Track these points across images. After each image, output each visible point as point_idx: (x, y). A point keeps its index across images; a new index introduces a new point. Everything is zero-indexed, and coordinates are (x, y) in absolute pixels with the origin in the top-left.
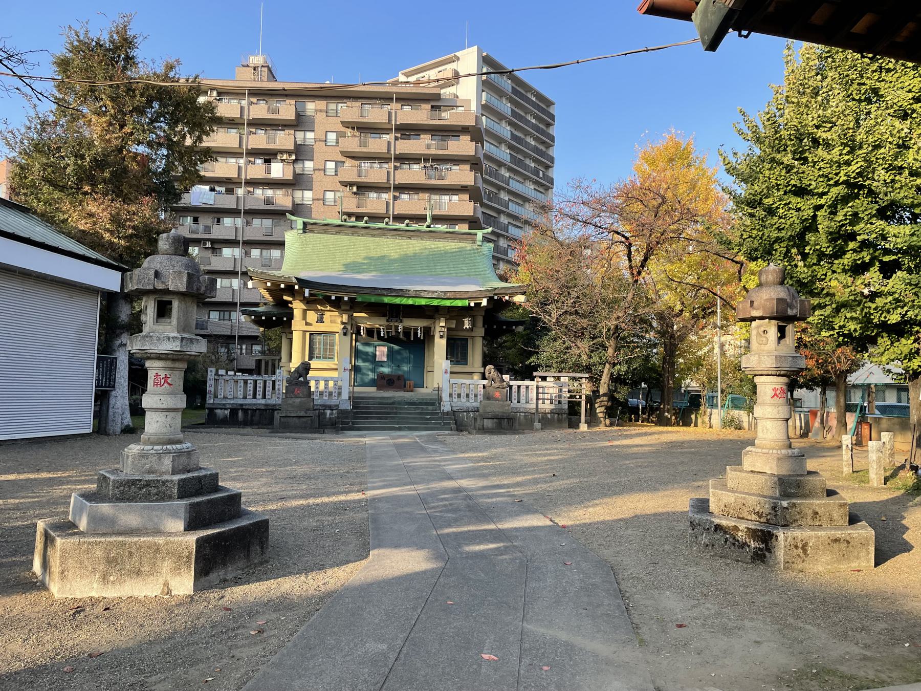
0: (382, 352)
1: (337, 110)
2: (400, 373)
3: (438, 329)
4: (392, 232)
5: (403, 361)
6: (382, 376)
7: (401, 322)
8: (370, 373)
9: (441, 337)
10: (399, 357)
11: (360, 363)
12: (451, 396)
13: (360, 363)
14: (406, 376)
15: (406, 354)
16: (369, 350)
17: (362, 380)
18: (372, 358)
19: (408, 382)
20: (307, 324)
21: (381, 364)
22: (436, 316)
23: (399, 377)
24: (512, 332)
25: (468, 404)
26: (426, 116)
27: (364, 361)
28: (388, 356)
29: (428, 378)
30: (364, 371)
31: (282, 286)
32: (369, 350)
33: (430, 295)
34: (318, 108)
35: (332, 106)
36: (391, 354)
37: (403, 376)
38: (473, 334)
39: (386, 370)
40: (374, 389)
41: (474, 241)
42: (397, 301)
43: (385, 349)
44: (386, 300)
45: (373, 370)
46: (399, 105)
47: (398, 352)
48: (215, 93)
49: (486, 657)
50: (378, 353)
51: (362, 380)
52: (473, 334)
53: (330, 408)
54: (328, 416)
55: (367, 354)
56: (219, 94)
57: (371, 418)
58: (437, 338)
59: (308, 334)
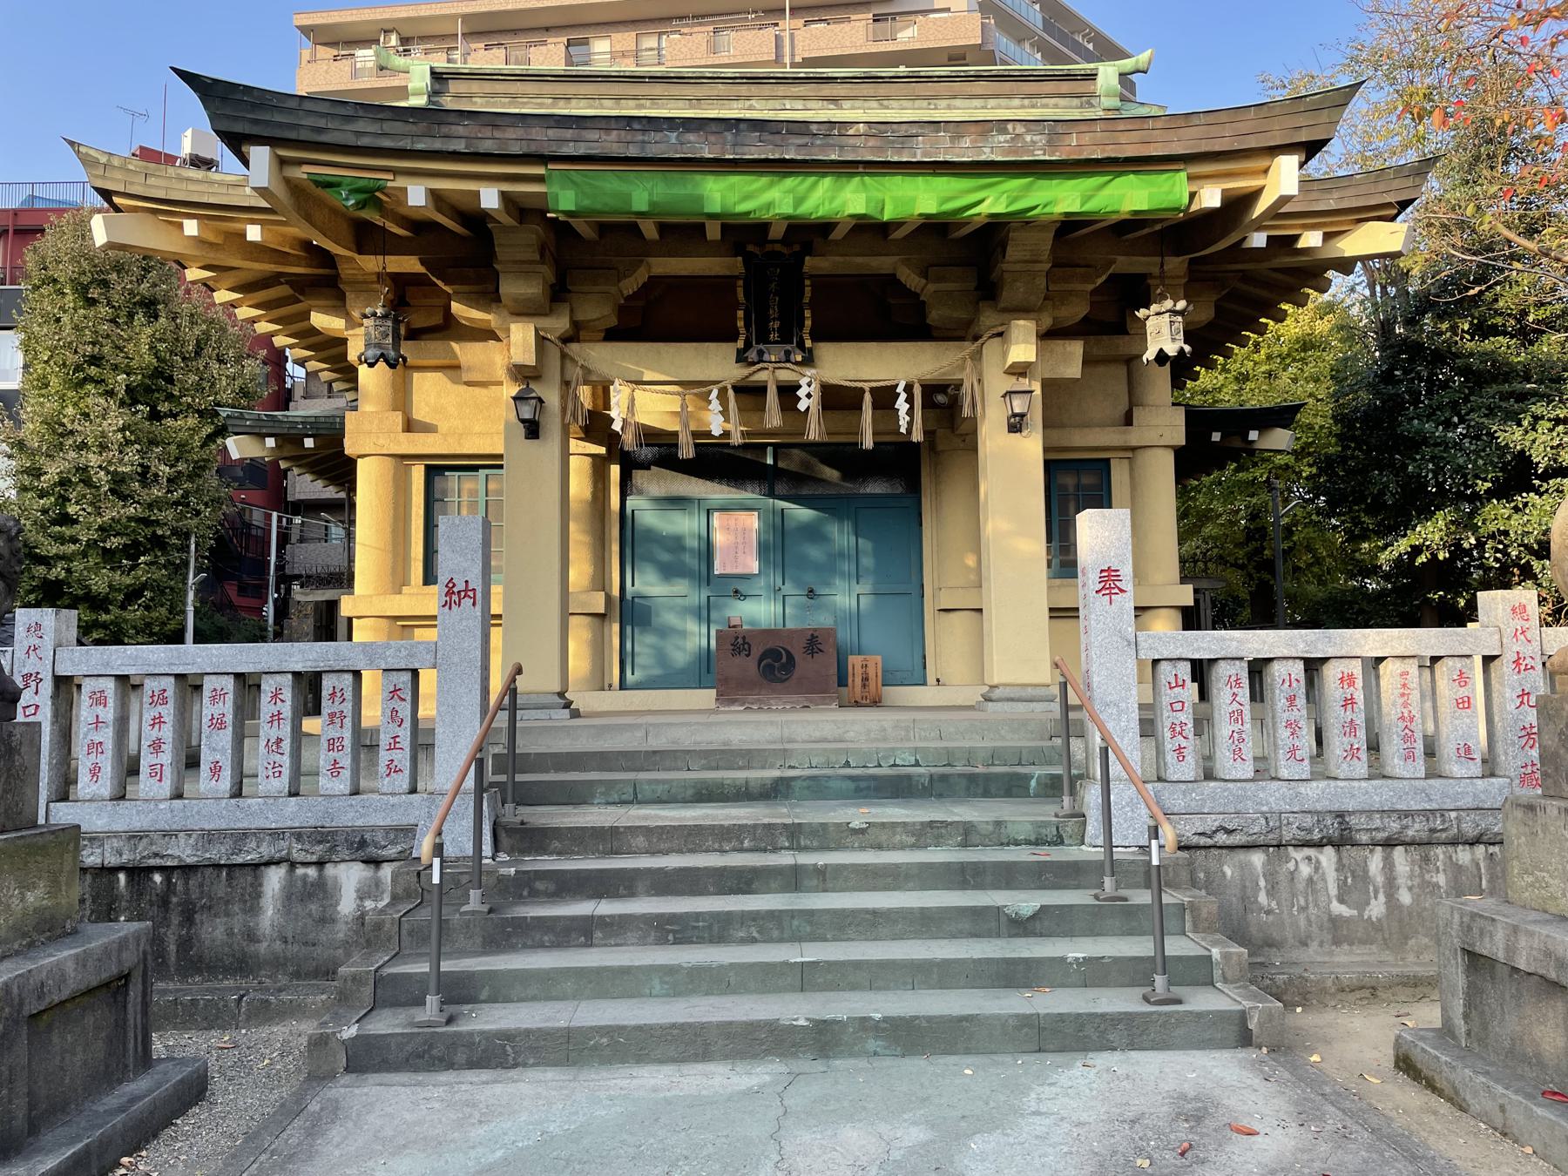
0: (735, 528)
1: (659, 49)
2: (823, 620)
3: (997, 383)
4: (766, 90)
5: (828, 569)
6: (737, 642)
7: (809, 361)
8: (692, 626)
9: (1016, 425)
10: (815, 552)
11: (647, 583)
12: (1148, 728)
13: (647, 583)
14: (845, 635)
15: (841, 535)
16: (684, 524)
17: (661, 658)
18: (696, 562)
19: (855, 661)
20: (410, 426)
21: (736, 587)
22: (988, 319)
23: (814, 642)
24: (1250, 454)
25: (1272, 796)
26: (862, 32)
27: (669, 572)
28: (764, 550)
29: (946, 643)
30: (671, 619)
31: (1299, 1010)
32: (684, 524)
33: (965, 150)
34: (618, 48)
35: (651, 42)
36: (778, 546)
37: (830, 633)
38: (1134, 437)
39: (759, 611)
40: (705, 697)
41: (1088, 98)
42: (774, 199)
43: (752, 521)
44: (723, 195)
45: (704, 614)
46: (800, 22)
47: (812, 533)
48: (394, 40)
49: (770, 461)
50: (719, 538)
51: (661, 658)
52: (1134, 437)
53: (363, 849)
54: (347, 905)
55: (676, 543)
56: (405, 41)
57: (615, 929)
58: (992, 437)
59: (418, 473)
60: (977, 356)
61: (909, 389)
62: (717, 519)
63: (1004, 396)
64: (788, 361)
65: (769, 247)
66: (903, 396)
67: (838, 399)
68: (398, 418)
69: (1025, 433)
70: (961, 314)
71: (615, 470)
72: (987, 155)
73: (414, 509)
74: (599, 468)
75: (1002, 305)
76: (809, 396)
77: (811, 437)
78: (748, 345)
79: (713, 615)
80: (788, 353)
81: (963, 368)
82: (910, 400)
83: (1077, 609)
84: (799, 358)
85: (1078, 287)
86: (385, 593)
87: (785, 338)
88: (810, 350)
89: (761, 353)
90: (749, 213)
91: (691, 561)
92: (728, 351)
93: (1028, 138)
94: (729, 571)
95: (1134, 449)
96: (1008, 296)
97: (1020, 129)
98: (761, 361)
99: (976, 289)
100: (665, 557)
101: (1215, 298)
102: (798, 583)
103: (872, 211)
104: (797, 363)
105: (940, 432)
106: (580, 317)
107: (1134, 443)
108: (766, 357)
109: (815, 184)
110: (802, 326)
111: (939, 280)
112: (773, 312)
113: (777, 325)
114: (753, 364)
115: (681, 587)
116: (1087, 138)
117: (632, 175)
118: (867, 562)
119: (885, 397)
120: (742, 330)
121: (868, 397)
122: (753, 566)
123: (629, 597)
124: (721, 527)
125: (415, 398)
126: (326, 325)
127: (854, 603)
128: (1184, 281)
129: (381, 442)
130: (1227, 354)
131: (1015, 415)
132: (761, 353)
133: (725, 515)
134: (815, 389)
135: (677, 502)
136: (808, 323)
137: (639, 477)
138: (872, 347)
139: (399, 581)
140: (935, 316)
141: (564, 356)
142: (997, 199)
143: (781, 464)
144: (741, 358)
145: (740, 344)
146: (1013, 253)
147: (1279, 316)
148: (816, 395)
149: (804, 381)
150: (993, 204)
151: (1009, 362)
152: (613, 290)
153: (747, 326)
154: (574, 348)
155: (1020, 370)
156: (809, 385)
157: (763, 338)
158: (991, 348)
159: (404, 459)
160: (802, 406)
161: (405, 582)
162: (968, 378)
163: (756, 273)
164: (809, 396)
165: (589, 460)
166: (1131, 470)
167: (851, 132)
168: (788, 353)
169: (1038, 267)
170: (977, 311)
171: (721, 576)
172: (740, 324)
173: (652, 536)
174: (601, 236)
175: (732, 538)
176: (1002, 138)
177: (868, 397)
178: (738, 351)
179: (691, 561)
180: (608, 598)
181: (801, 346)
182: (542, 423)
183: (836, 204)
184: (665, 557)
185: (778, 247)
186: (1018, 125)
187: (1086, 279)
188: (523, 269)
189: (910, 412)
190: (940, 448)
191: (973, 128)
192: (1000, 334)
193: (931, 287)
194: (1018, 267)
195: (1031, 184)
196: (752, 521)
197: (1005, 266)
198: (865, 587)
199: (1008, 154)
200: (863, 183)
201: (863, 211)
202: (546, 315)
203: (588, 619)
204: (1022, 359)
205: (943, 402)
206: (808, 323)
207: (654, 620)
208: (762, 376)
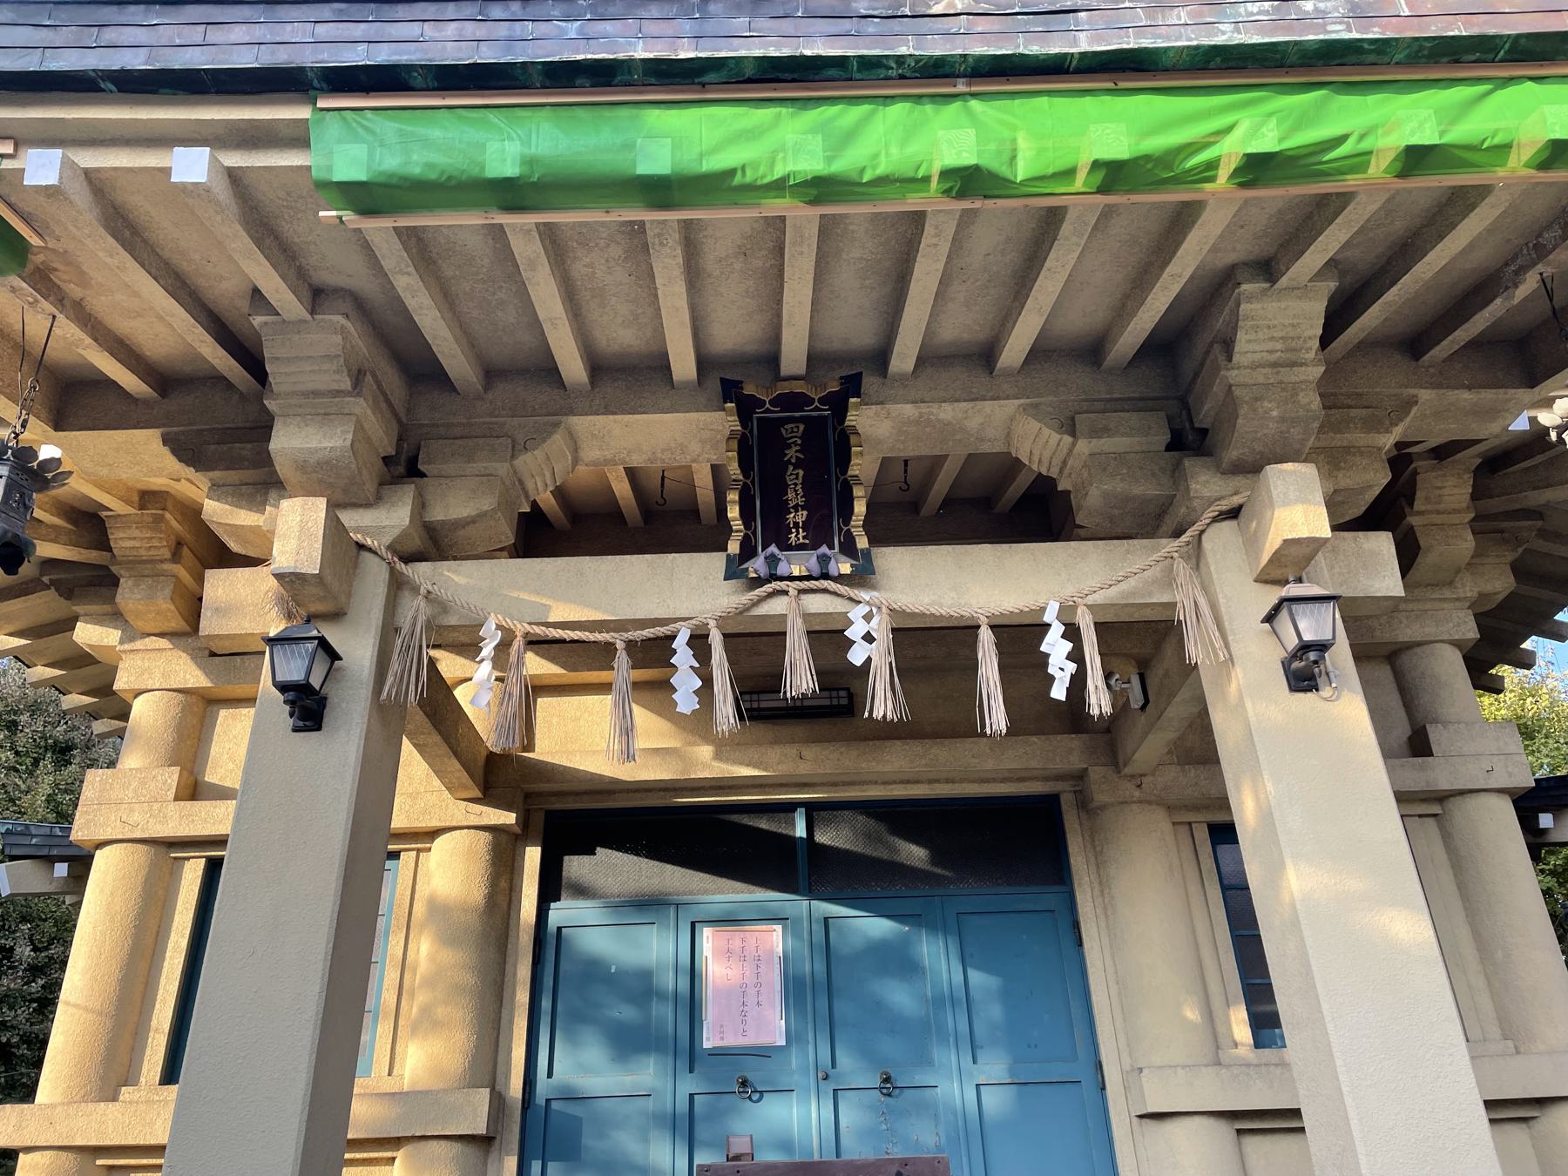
5: (921, 1035)
7: (863, 576)
10: (899, 996)
11: (582, 1067)
16: (652, 948)
18: (664, 1021)
21: (744, 1075)
22: (1207, 485)
27: (628, 1043)
28: (796, 990)
32: (652, 948)
49: (800, 831)
55: (640, 986)
60: (1196, 554)
62: (707, 935)
63: (1269, 619)
64: (825, 576)
65: (784, 388)
66: (1057, 630)
67: (931, 649)
69: (1326, 692)
70: (1147, 488)
73: (173, 937)
74: (504, 850)
75: (1232, 454)
76: (869, 638)
77: (878, 713)
78: (748, 552)
79: (701, 1132)
80: (823, 560)
81: (1169, 580)
82: (1072, 633)
83: (1296, 1113)
84: (845, 568)
85: (1359, 438)
86: (84, 1099)
87: (819, 534)
88: (867, 554)
89: (772, 561)
90: (732, 172)
91: (663, 1012)
94: (732, 1040)
95: (1442, 797)
98: (774, 577)
100: (625, 1013)
102: (867, 1053)
104: (840, 579)
105: (1096, 773)
106: (439, 513)
107: (1444, 783)
109: (865, 120)
110: (847, 512)
112: (794, 496)
113: (802, 516)
114: (758, 582)
115: (647, 1074)
119: (1021, 638)
120: (737, 525)
121: (986, 637)
122: (772, 1026)
124: (715, 951)
125: (215, 749)
129: (135, 817)
130: (1525, 661)
131: (1305, 647)
132: (772, 561)
133: (734, 937)
134: (880, 627)
135: (648, 905)
136: (860, 508)
137: (576, 866)
139: (112, 1075)
141: (398, 584)
143: (822, 838)
144: (734, 571)
145: (734, 547)
148: (883, 637)
150: (1255, 131)
151: (1272, 543)
152: (502, 468)
153: (747, 515)
154: (421, 572)
155: (1294, 560)
156: (868, 617)
157: (778, 534)
158: (1221, 541)
159: (172, 847)
160: (857, 657)
161: (129, 1077)
162: (1185, 598)
163: (760, 447)
164: (869, 638)
165: (486, 837)
166: (1447, 837)
170: (1177, 475)
171: (718, 1053)
173: (596, 972)
175: (360, 406)
177: (986, 637)
179: (663, 1012)
180: (498, 1102)
181: (849, 549)
184: (625, 1013)
185: (799, 387)
189: (1077, 656)
190: (1100, 797)
192: (1234, 514)
193: (1084, 447)
194: (1260, 376)
196: (775, 938)
197: (1233, 376)
198: (994, 1067)
199: (1273, 32)
200: (970, 114)
202: (367, 505)
203: (456, 1147)
204: (1304, 533)
205: (1144, 645)
206: (860, 508)
207: (589, 1141)
208: (777, 606)
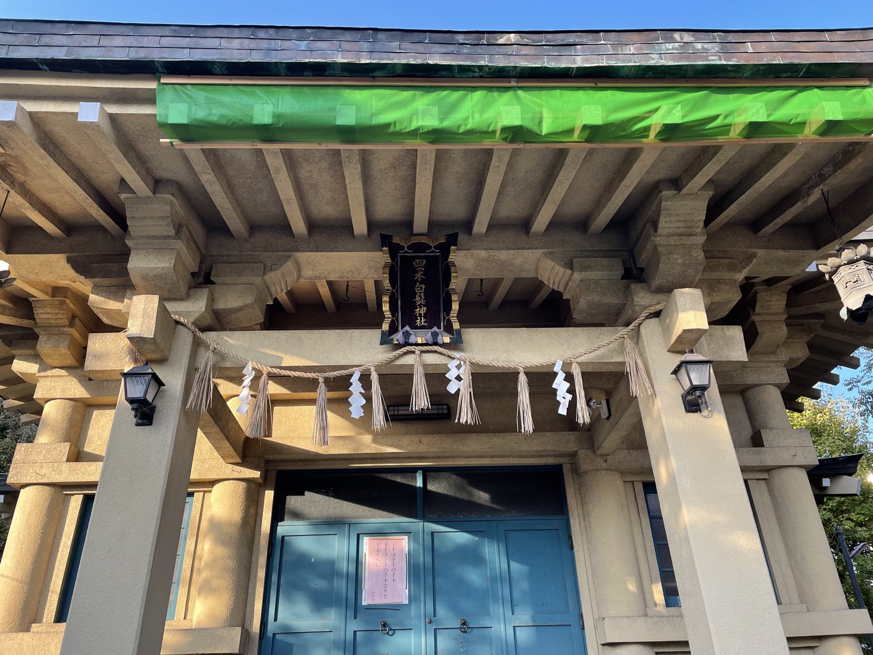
5: (483, 599)
7: (456, 344)
16: (335, 548)
18: (340, 588)
27: (321, 601)
28: (415, 572)
36: (426, 573)
49: (419, 483)
55: (328, 569)
60: (637, 336)
61: (566, 367)
62: (366, 541)
63: (675, 372)
64: (436, 344)
65: (415, 240)
66: (561, 376)
67: (493, 385)
68: (66, 448)
69: (705, 413)
70: (611, 300)
71: (269, 496)
72: (654, 60)
76: (459, 378)
77: (463, 420)
78: (393, 329)
80: (435, 335)
81: (622, 350)
82: (569, 378)
84: (447, 339)
85: (726, 275)
86: (11, 631)
87: (433, 320)
88: (459, 332)
89: (407, 335)
92: (374, 335)
93: (699, 46)
94: (378, 601)
95: (769, 470)
96: (664, 271)
97: (688, 38)
98: (407, 344)
99: (623, 278)
101: (806, 339)
102: (454, 608)
103: (528, 124)
104: (444, 345)
105: (583, 453)
108: (412, 339)
110: (448, 309)
111: (584, 268)
112: (419, 299)
113: (423, 310)
114: (399, 346)
116: (763, 47)
117: (257, 90)
118: (523, 586)
119: (542, 381)
120: (388, 314)
121: (523, 379)
123: (270, 633)
125: (91, 432)
126: (24, 370)
127: (510, 631)
128: (785, 316)
129: (44, 471)
131: (694, 388)
132: (407, 335)
134: (465, 372)
136: (455, 306)
137: (293, 502)
138: (523, 333)
140: (581, 306)
141: (197, 344)
142: (670, 111)
144: (385, 340)
145: (386, 327)
146: (666, 225)
147: (854, 362)
149: (452, 364)
151: (677, 331)
152: (258, 280)
153: (393, 309)
154: (211, 337)
156: (459, 367)
157: (410, 320)
158: (650, 329)
161: (37, 618)
162: (630, 360)
163: (401, 272)
164: (459, 378)
165: (243, 485)
167: (501, 41)
168: (435, 335)
169: (693, 240)
170: (627, 293)
171: (369, 608)
172: (386, 308)
173: (304, 561)
174: (251, 235)
176: (670, 46)
177: (523, 379)
178: (383, 333)
180: (246, 635)
181: (449, 329)
182: (158, 403)
183: (489, 115)
185: (424, 240)
186: (685, 35)
187: (732, 268)
188: (155, 243)
189: (571, 391)
190: (584, 467)
191: (636, 37)
192: (657, 314)
193: (577, 276)
195: (706, 95)
196: (404, 543)
197: (657, 240)
198: (524, 616)
199: (680, 59)
200: (518, 98)
201: (517, 122)
204: (694, 326)
206: (455, 306)
208: (409, 360)
